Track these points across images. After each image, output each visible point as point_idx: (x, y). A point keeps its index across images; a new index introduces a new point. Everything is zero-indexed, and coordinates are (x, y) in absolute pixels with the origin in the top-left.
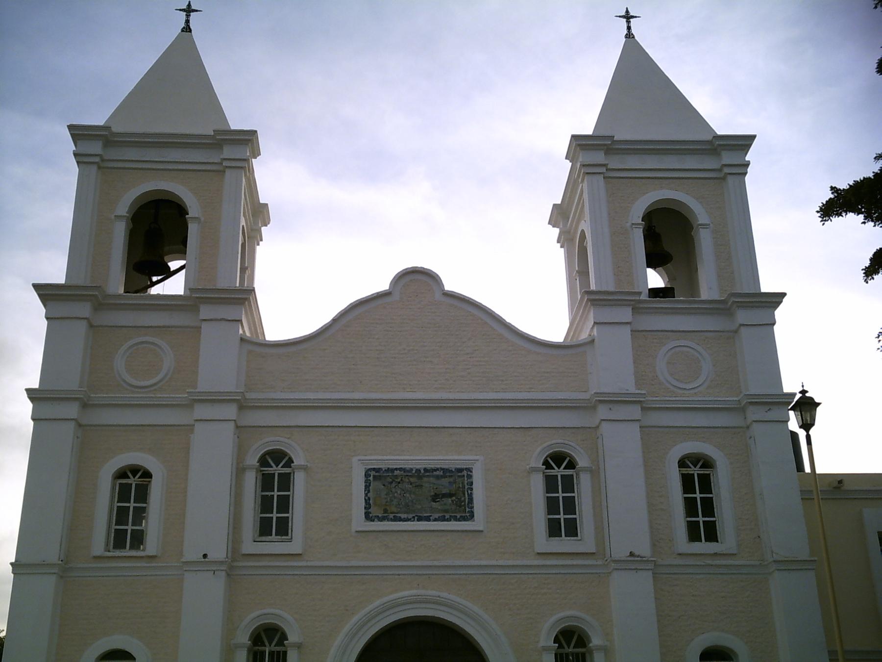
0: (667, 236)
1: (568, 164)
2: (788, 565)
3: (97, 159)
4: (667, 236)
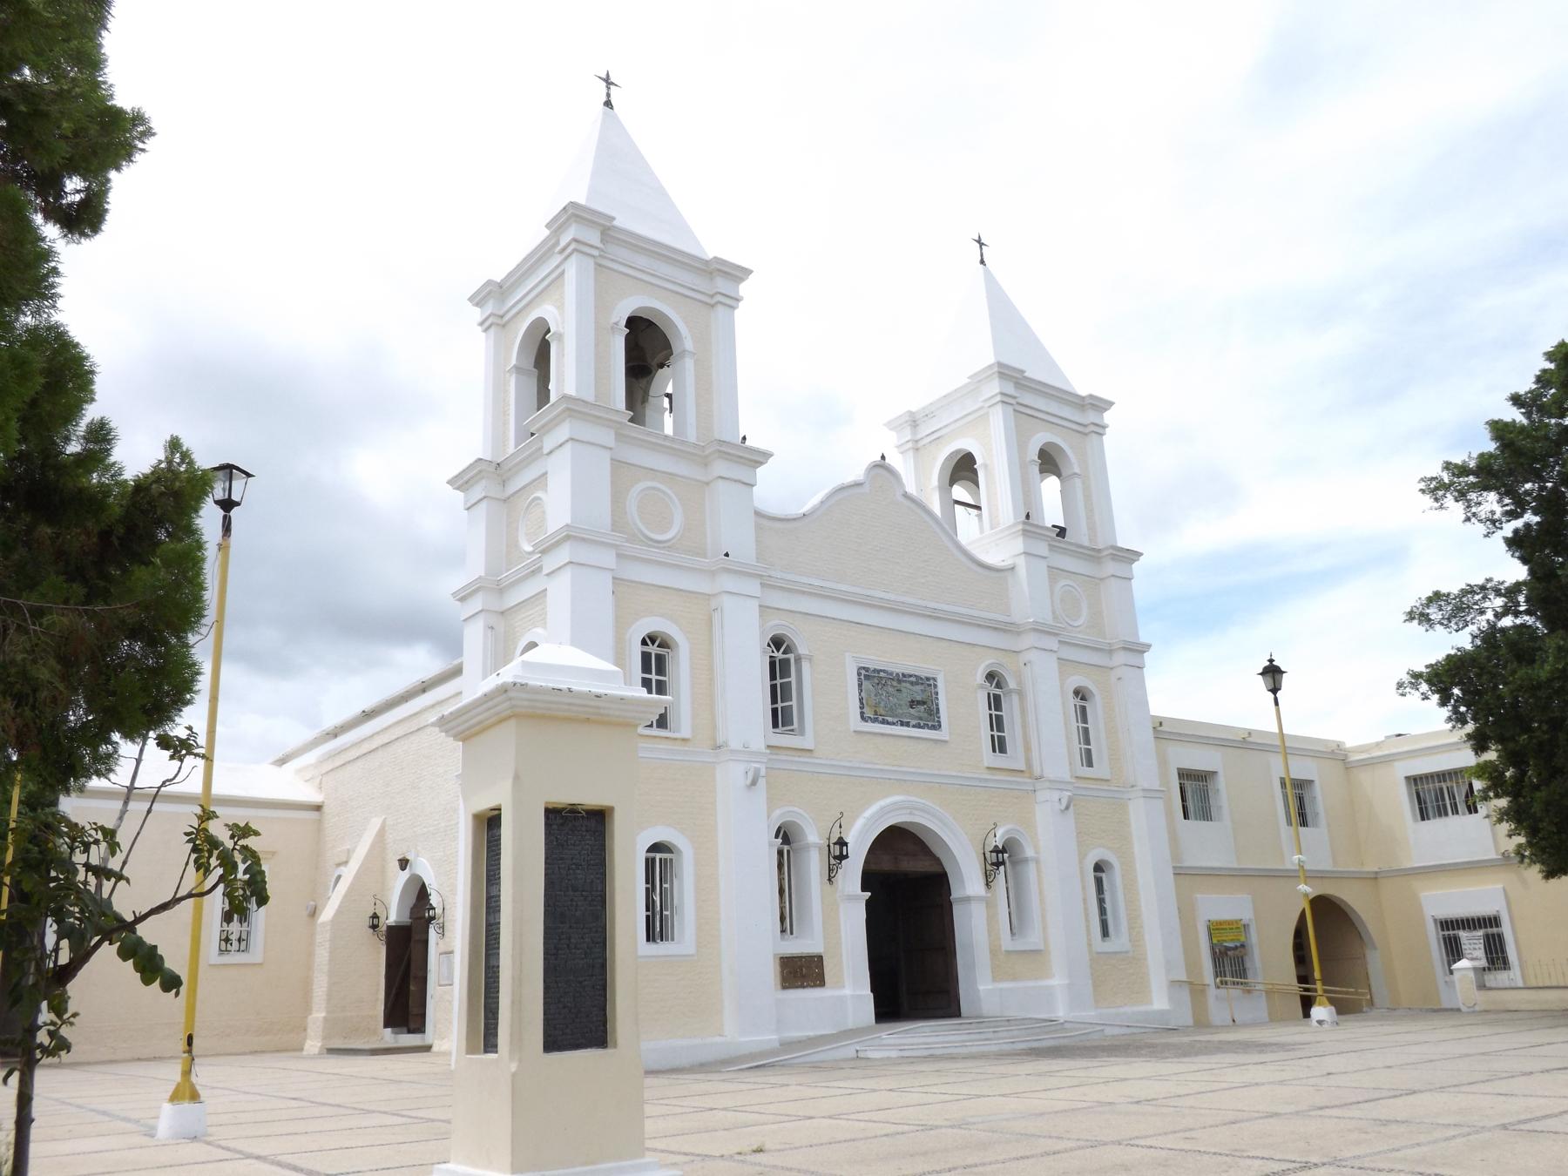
0: (786, 840)
2: (1149, 794)
3: (596, 253)
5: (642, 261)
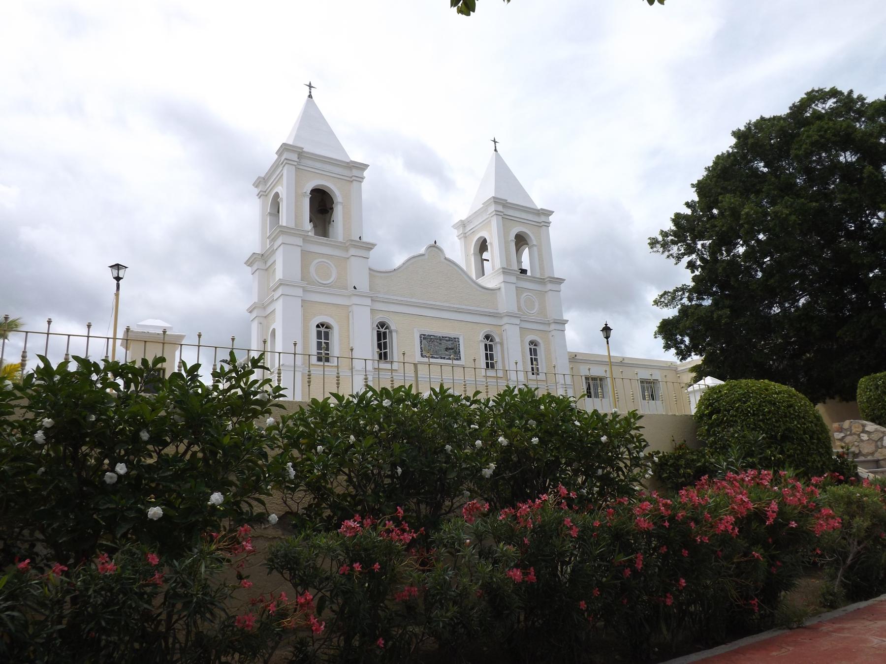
1: (276, 156)
4: (322, 205)
5: (318, 165)
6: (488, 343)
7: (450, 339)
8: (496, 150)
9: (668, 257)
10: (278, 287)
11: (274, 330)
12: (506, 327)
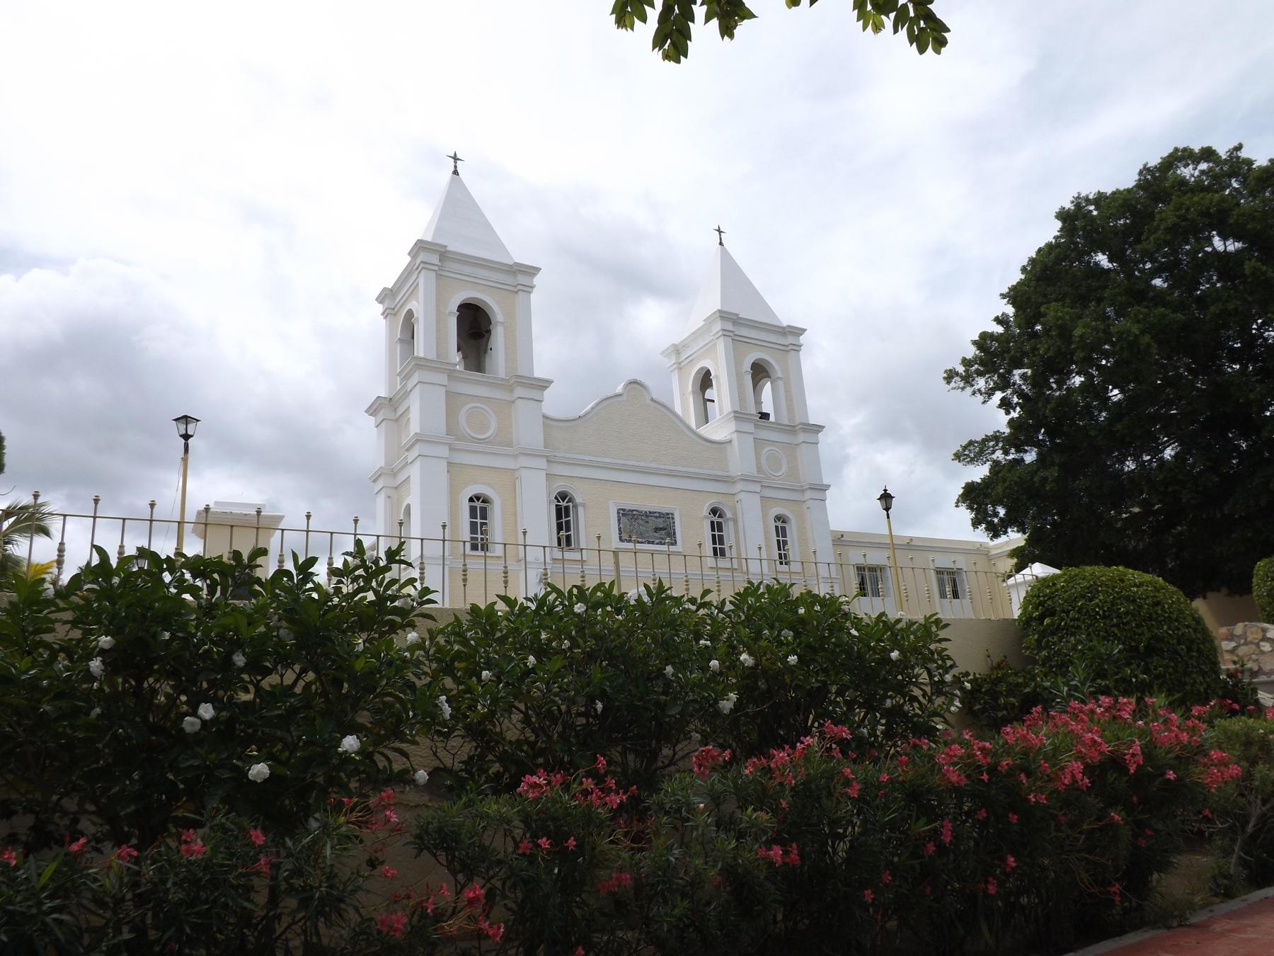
1: (409, 259)
4: (474, 326)
5: (468, 270)
6: (716, 519)
7: (661, 515)
8: (721, 244)
9: (974, 393)
10: (413, 445)
11: (408, 507)
12: (741, 496)
